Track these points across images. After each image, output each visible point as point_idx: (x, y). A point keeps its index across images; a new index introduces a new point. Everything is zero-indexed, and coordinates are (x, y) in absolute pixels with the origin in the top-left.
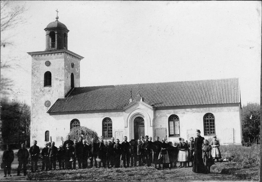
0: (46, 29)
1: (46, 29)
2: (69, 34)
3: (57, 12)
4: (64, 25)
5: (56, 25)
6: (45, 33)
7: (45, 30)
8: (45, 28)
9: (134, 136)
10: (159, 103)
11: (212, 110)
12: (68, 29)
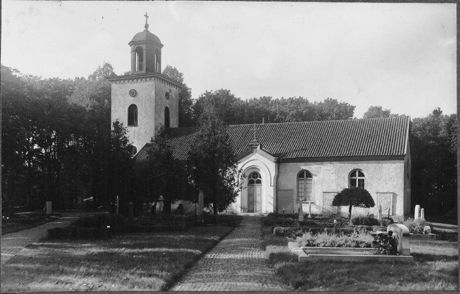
0: (131, 44)
1: (131, 44)
2: (163, 50)
3: (145, 18)
4: (157, 37)
5: (143, 38)
6: (129, 49)
7: (129, 44)
8: (129, 42)
9: (402, 204)
10: (299, 151)
11: (362, 166)
12: (162, 43)
